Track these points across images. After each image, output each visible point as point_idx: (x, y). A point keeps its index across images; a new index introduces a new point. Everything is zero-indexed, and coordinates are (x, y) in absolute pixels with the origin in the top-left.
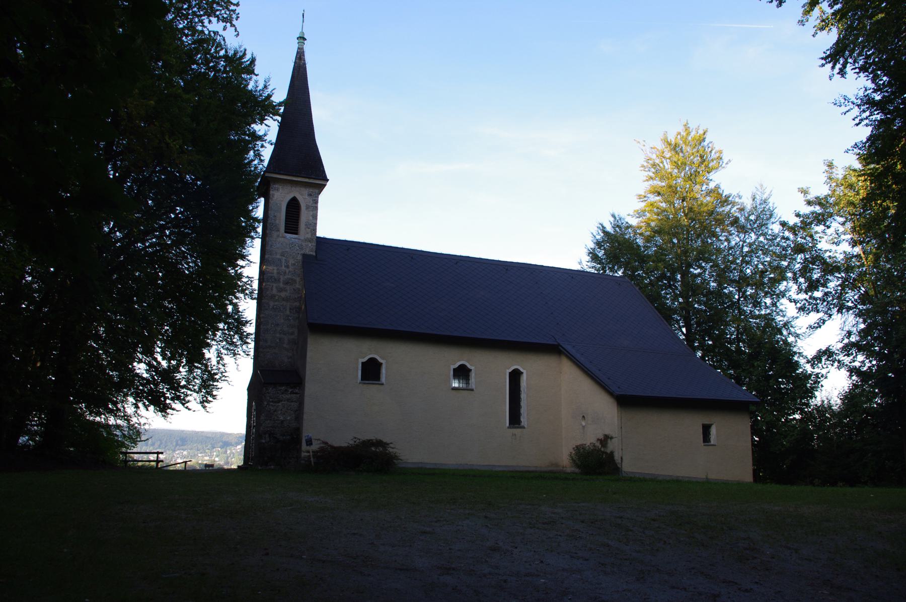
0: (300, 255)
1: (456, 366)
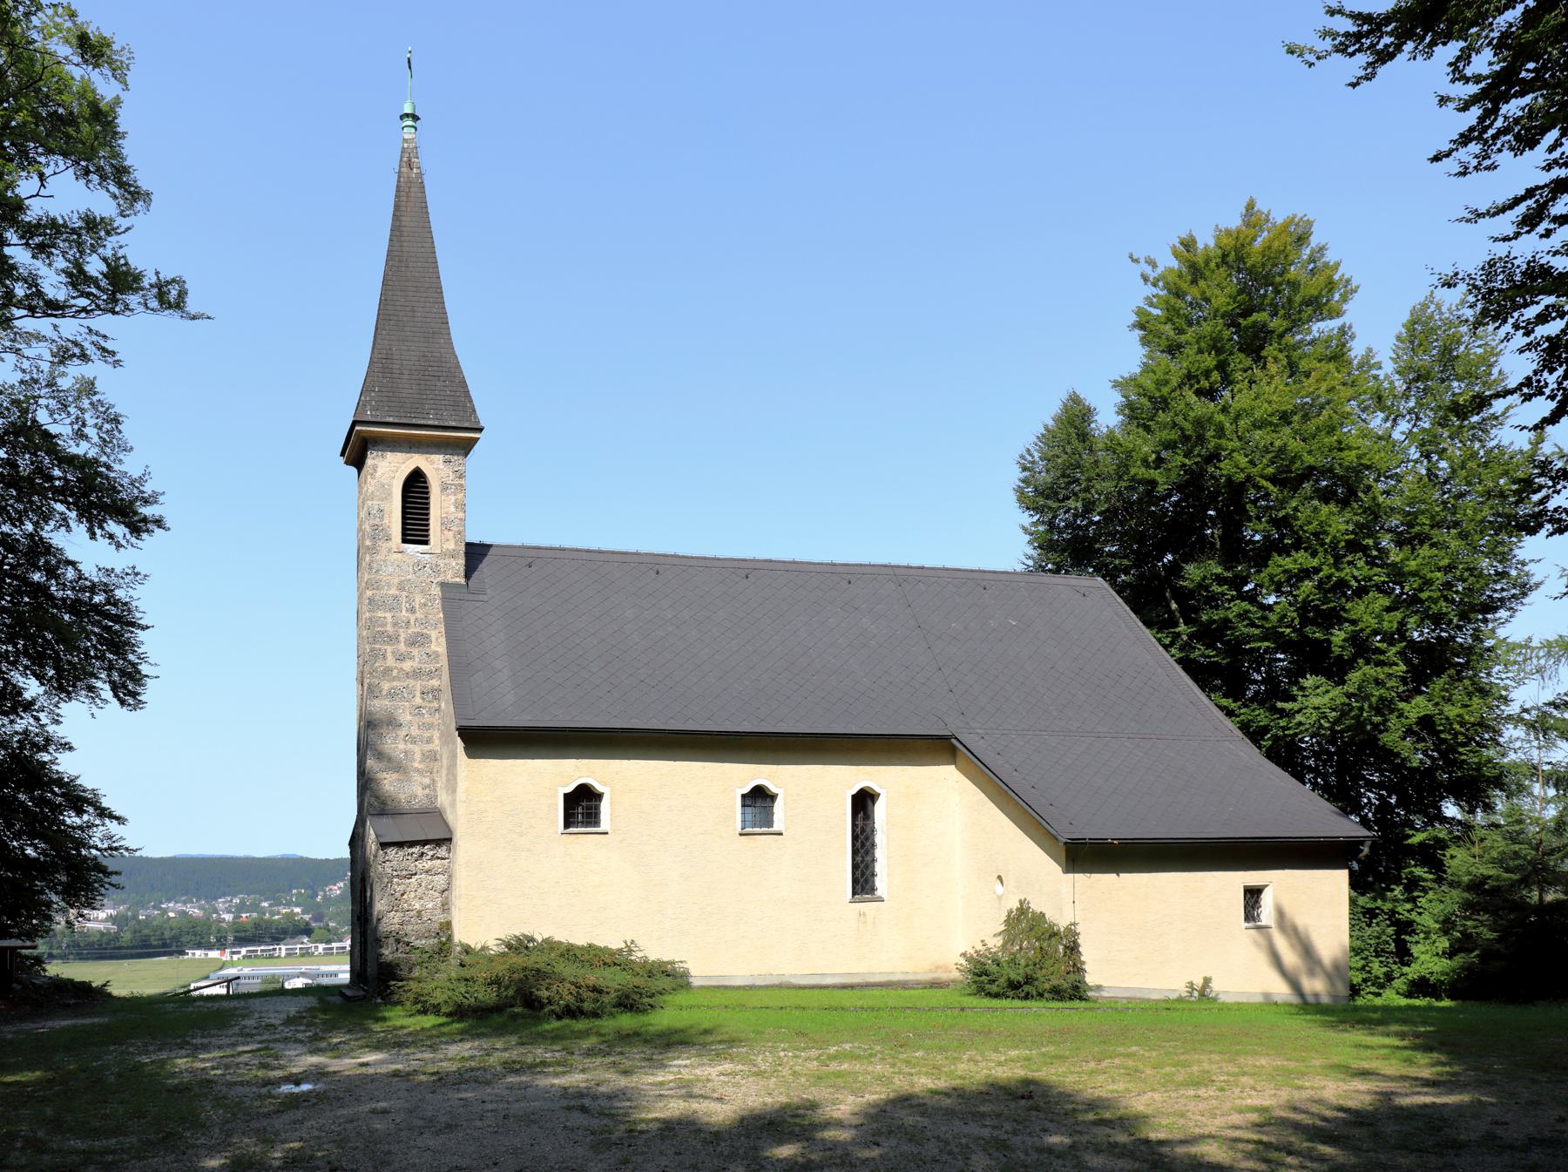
0: (434, 585)
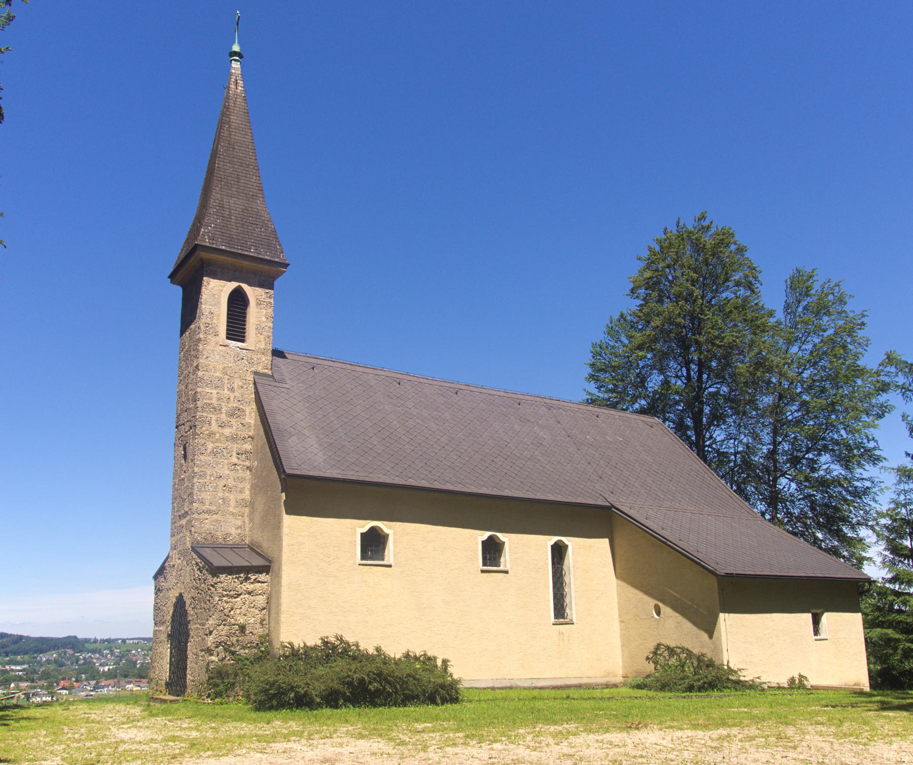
0: (249, 373)
1: (365, 530)
